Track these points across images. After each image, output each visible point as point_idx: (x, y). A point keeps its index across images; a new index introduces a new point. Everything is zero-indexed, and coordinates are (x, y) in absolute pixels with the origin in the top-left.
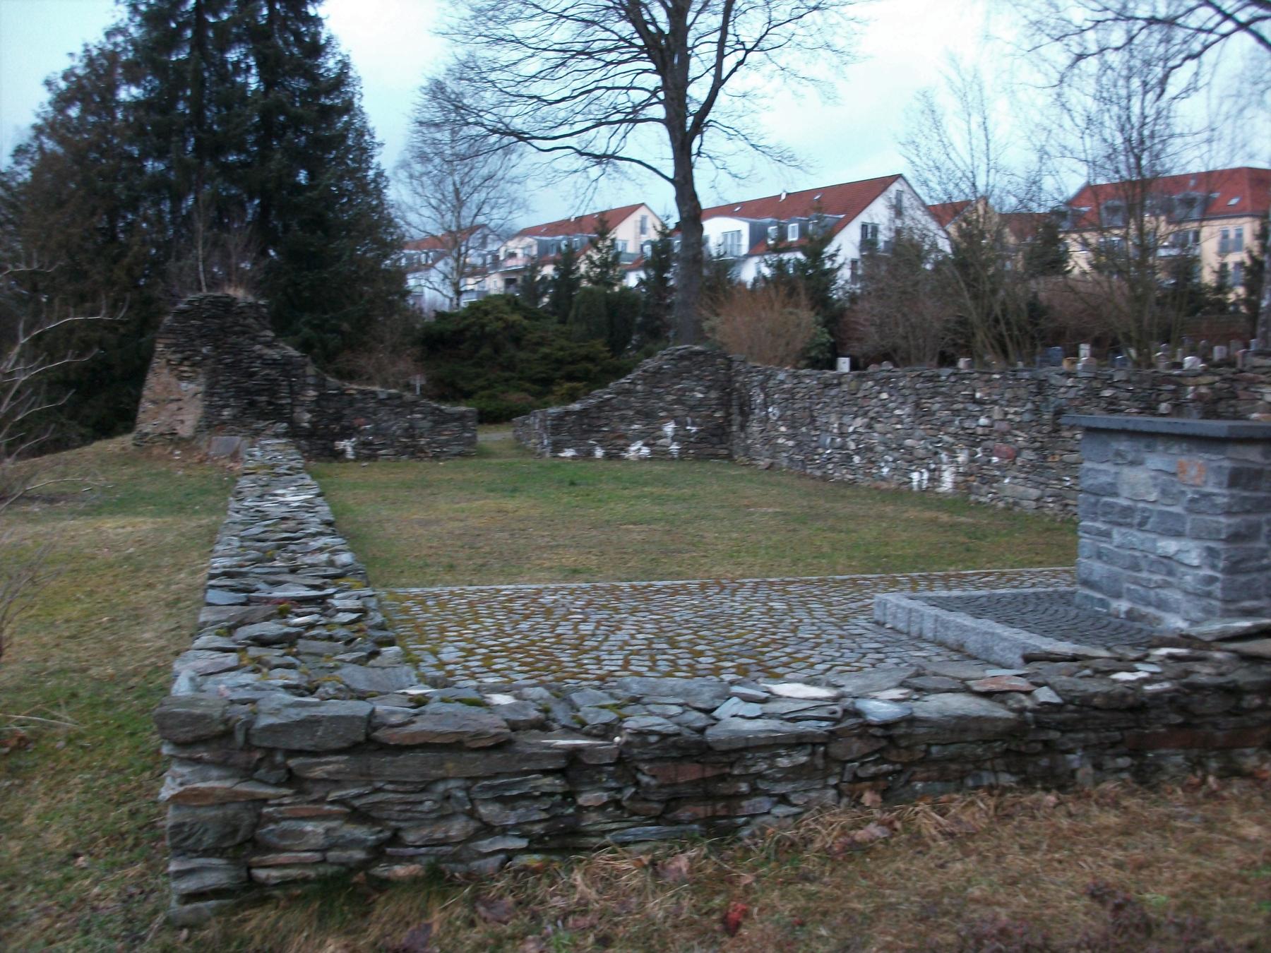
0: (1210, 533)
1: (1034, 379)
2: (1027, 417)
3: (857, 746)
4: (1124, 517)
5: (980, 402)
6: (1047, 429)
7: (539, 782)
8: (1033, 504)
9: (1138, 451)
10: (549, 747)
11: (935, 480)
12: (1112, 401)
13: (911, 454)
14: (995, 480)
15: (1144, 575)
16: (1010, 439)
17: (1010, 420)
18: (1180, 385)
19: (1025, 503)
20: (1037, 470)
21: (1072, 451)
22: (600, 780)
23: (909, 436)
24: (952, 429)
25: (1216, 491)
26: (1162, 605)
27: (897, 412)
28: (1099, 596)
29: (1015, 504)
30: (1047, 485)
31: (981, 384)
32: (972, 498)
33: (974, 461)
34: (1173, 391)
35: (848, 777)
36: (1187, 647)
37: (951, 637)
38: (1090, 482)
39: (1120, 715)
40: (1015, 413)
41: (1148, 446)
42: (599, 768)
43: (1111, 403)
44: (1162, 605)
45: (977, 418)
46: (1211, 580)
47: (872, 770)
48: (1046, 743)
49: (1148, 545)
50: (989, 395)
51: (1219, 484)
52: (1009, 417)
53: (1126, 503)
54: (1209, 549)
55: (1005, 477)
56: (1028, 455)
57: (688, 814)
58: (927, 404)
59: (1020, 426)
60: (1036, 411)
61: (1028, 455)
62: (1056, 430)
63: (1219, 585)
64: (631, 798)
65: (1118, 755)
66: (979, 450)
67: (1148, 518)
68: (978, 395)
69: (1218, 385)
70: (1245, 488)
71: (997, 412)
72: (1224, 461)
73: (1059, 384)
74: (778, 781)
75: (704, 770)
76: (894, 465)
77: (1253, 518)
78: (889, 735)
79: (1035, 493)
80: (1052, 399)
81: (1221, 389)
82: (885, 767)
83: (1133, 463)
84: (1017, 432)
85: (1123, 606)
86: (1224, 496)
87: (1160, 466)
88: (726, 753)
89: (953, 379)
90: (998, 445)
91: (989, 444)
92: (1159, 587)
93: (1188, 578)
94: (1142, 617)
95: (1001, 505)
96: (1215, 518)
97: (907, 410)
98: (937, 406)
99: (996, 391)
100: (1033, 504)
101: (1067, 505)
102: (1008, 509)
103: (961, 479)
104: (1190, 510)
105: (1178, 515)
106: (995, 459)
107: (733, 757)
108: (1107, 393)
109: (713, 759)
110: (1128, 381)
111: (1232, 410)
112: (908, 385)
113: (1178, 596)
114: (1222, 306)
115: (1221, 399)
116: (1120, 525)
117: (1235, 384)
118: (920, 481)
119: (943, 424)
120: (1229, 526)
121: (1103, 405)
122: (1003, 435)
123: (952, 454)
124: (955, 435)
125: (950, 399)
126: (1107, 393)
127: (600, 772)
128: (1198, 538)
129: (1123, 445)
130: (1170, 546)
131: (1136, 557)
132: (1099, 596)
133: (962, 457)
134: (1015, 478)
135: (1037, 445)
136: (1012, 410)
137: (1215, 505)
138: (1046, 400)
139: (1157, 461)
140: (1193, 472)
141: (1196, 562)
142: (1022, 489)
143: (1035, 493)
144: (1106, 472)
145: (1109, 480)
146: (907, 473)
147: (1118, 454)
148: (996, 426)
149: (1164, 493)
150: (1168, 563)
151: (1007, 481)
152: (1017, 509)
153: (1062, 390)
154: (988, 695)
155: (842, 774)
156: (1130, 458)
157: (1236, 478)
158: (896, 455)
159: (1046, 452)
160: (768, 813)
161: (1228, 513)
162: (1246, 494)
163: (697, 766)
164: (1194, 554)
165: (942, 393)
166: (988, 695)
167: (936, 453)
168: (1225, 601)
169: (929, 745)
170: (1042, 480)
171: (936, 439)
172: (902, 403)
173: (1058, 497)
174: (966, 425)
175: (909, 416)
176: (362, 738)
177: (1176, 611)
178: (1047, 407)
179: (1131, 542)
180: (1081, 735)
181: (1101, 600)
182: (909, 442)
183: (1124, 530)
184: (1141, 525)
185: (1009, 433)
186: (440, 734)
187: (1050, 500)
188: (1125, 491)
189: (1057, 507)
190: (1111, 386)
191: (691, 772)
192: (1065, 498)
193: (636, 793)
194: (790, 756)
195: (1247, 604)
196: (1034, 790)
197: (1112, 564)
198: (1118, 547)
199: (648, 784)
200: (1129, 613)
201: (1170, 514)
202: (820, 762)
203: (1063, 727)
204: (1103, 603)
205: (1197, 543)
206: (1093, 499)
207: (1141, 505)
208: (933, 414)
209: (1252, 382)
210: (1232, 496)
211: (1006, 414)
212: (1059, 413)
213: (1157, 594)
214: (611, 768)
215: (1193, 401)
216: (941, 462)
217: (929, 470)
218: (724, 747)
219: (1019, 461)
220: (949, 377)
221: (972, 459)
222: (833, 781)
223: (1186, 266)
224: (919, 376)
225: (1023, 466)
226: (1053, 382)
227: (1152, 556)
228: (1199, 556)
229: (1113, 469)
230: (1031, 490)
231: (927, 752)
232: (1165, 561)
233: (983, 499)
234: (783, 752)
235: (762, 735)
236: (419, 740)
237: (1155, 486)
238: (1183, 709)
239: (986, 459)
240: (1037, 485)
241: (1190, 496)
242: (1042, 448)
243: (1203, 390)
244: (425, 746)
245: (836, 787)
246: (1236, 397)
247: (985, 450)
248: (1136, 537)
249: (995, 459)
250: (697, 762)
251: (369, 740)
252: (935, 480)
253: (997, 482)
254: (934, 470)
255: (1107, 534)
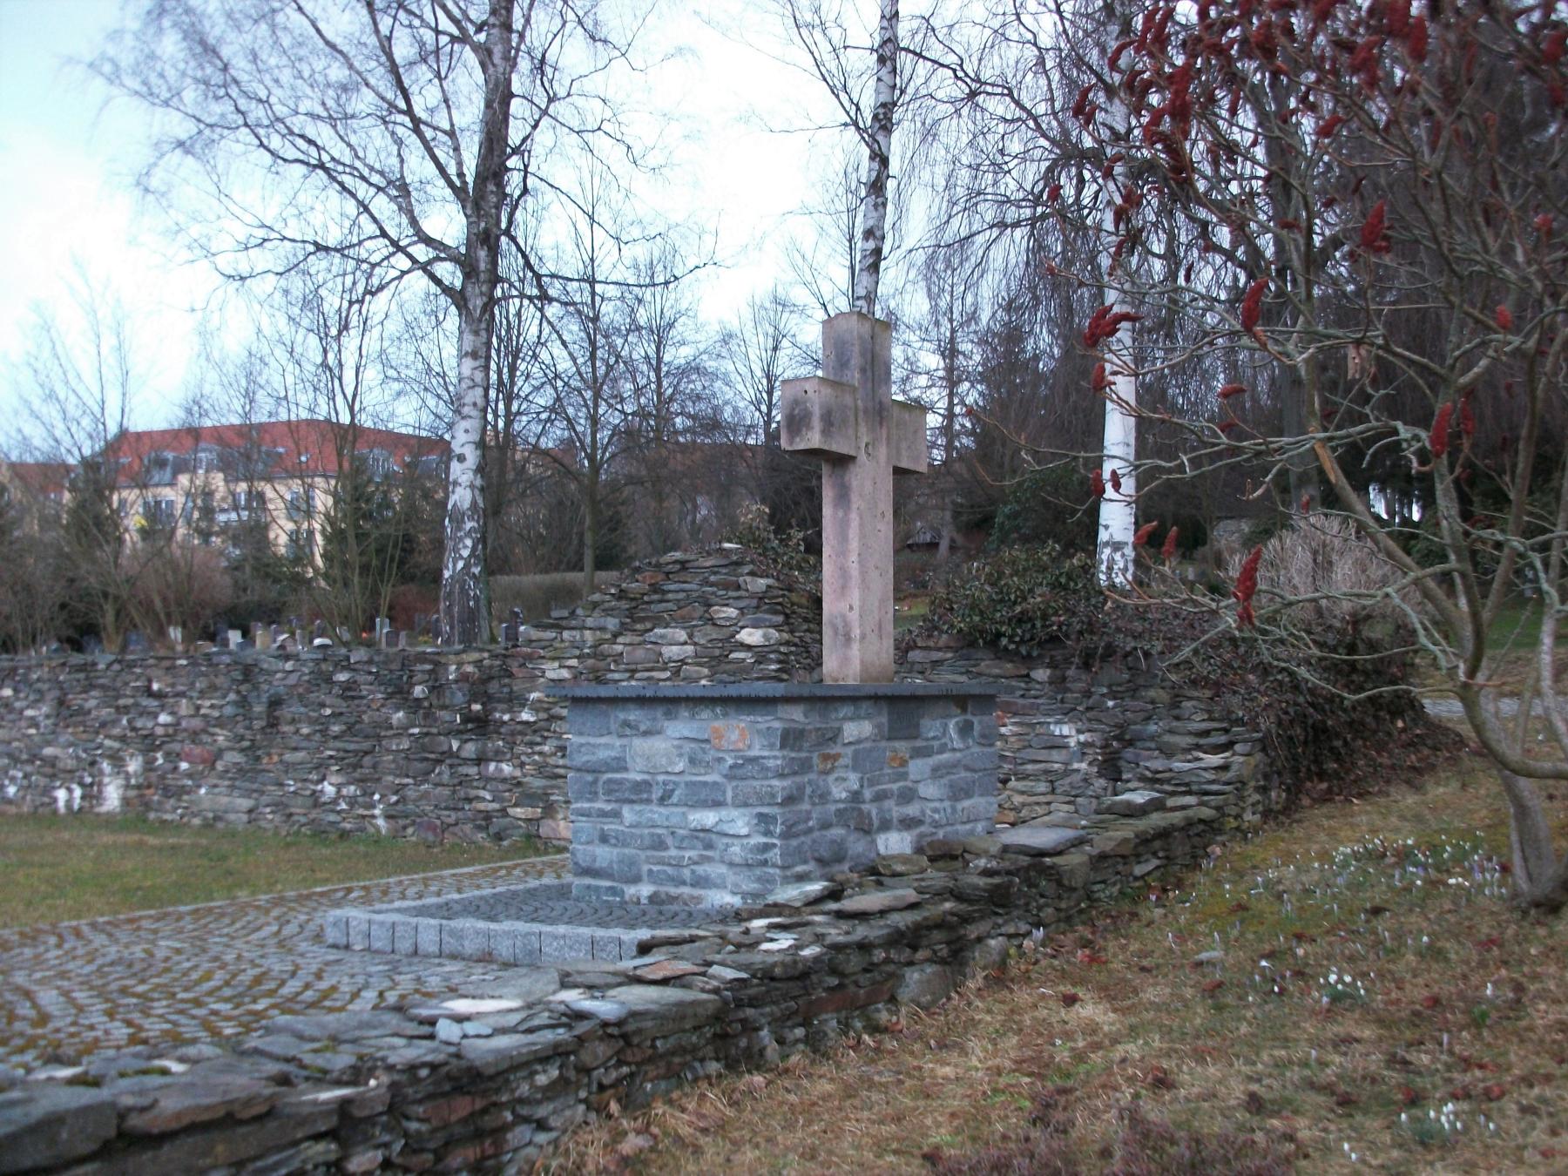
0: (760, 798)
1: (236, 663)
2: (229, 710)
3: (602, 1050)
4: (640, 792)
5: (159, 695)
6: (257, 724)
7: (310, 1152)
8: (245, 818)
9: (654, 719)
10: (315, 1103)
11: (92, 797)
12: (348, 687)
13: (53, 766)
14: (184, 790)
15: (673, 852)
16: (205, 738)
17: (204, 716)
18: (437, 664)
19: (232, 817)
20: (246, 775)
21: (295, 749)
22: (373, 1136)
23: (49, 743)
24: (116, 731)
25: (766, 753)
26: (701, 882)
27: (29, 713)
28: (608, 883)
29: (216, 818)
30: (263, 793)
31: (160, 673)
32: (152, 816)
33: (151, 770)
34: (430, 672)
35: (594, 1087)
36: (779, 915)
37: (469, 947)
38: (585, 758)
39: (791, 984)
40: (212, 707)
41: (665, 714)
42: (371, 1120)
43: (350, 689)
44: (701, 882)
45: (156, 716)
46: (767, 847)
47: (614, 1075)
48: (744, 1021)
49: (674, 820)
50: (173, 685)
51: (771, 746)
52: (203, 711)
53: (639, 777)
54: (761, 816)
55: (199, 787)
56: (233, 757)
57: (459, 1160)
58: (75, 700)
59: (220, 722)
60: (243, 702)
61: (233, 757)
62: (273, 723)
63: (777, 851)
64: (401, 1153)
65: (794, 1027)
66: (159, 755)
67: (673, 791)
68: (155, 686)
69: (486, 662)
70: (792, 750)
71: (184, 707)
72: (773, 722)
73: (274, 668)
74: (539, 1102)
75: (473, 1102)
76: (25, 782)
77: (798, 779)
78: (621, 1033)
79: (246, 803)
80: (265, 687)
81: (491, 667)
82: (625, 1070)
83: (646, 734)
84: (217, 730)
85: (645, 890)
86: (775, 758)
87: (686, 733)
88: (491, 1078)
89: (116, 667)
90: (188, 747)
91: (176, 747)
92: (695, 863)
93: (736, 849)
94: (673, 899)
95: (196, 821)
96: (766, 783)
97: (45, 709)
98: (92, 703)
99: (184, 680)
100: (245, 818)
101: (291, 815)
102: (208, 825)
103: (132, 793)
104: (729, 777)
105: (715, 783)
106: (184, 766)
107: (500, 1080)
108: (342, 677)
109: (483, 1086)
110: (370, 662)
111: (506, 690)
112: (46, 676)
113: (723, 869)
114: (299, 581)
115: (491, 678)
116: (632, 802)
117: (509, 661)
118: (69, 803)
119: (103, 725)
120: (784, 789)
121: (336, 690)
122: (194, 736)
123: (117, 760)
124: (122, 739)
125: (112, 694)
126: (342, 677)
127: (374, 1125)
128: (746, 805)
129: (633, 714)
130: (709, 818)
131: (659, 836)
132: (608, 883)
133: (134, 765)
134: (215, 786)
135: (246, 744)
136: (208, 703)
137: (768, 769)
138: (256, 687)
139: (681, 727)
140: (734, 736)
141: (744, 831)
142: (225, 800)
143: (246, 803)
144: (606, 746)
145: (613, 754)
146: (48, 791)
147: (626, 724)
148: (184, 724)
149: (692, 761)
150: (705, 837)
151: (203, 791)
152: (220, 825)
153: (279, 675)
154: (664, 982)
155: (589, 1085)
156: (643, 728)
157: (790, 738)
158: (29, 768)
159: (259, 753)
160: (530, 1143)
161: (782, 776)
162: (793, 755)
163: (468, 1099)
164: (740, 823)
165: (102, 687)
166: (664, 982)
167: (93, 763)
168: (783, 868)
169: (654, 1040)
170: (255, 786)
171: (93, 745)
172: (37, 701)
173: (278, 806)
174: (139, 724)
175: (47, 717)
176: (113, 1133)
177: (721, 886)
178: (259, 696)
179: (651, 819)
180: (768, 1009)
181: (611, 888)
182: (48, 751)
183: (637, 807)
184: (662, 800)
185: (204, 731)
186: (208, 1108)
187: (268, 810)
188: (640, 764)
189: (278, 818)
190: (348, 667)
191: (463, 1106)
192: (287, 806)
193: (406, 1144)
194: (545, 1071)
195: (800, 869)
196: (740, 1075)
197: (625, 845)
198: (631, 826)
199: (418, 1132)
200: (653, 899)
201: (705, 784)
202: (572, 1074)
203: (754, 1002)
204: (612, 891)
205: (742, 810)
206: (590, 778)
207: (661, 778)
208: (89, 712)
209: (530, 658)
210: (784, 757)
211: (198, 708)
212: (275, 703)
213: (693, 872)
214: (384, 1118)
215: (456, 681)
216: (101, 773)
217: (82, 784)
218: (492, 1071)
219: (220, 766)
220: (109, 665)
221: (149, 766)
222: (583, 1094)
223: (255, 533)
224: (64, 664)
225: (227, 771)
226: (265, 666)
227: (681, 832)
228: (748, 824)
229: (618, 742)
230: (239, 801)
231: (653, 1046)
232: (701, 835)
233: (168, 817)
234: (539, 1068)
235: (524, 1050)
236: (185, 1121)
237: (680, 755)
238: (834, 971)
239: (169, 766)
240: (248, 794)
241: (730, 762)
242: (253, 746)
243: (469, 669)
244: (193, 1128)
245: (585, 1101)
246: (511, 675)
247: (167, 755)
248: (657, 813)
249: (184, 766)
250: (469, 1093)
251: (121, 1134)
252: (92, 797)
253: (188, 793)
254: (92, 785)
255: (617, 814)
